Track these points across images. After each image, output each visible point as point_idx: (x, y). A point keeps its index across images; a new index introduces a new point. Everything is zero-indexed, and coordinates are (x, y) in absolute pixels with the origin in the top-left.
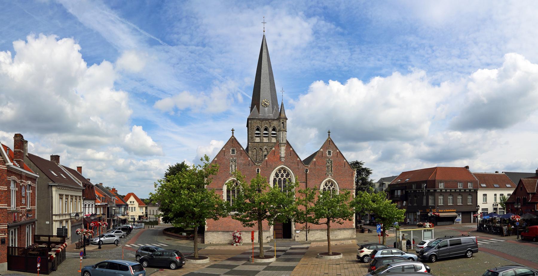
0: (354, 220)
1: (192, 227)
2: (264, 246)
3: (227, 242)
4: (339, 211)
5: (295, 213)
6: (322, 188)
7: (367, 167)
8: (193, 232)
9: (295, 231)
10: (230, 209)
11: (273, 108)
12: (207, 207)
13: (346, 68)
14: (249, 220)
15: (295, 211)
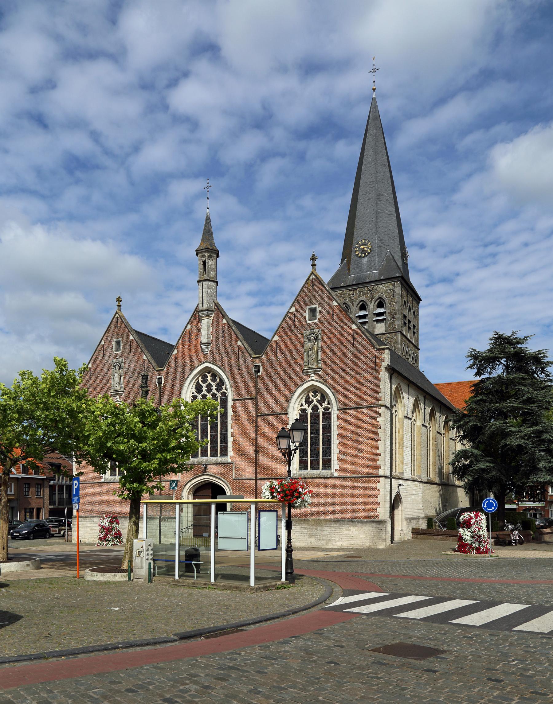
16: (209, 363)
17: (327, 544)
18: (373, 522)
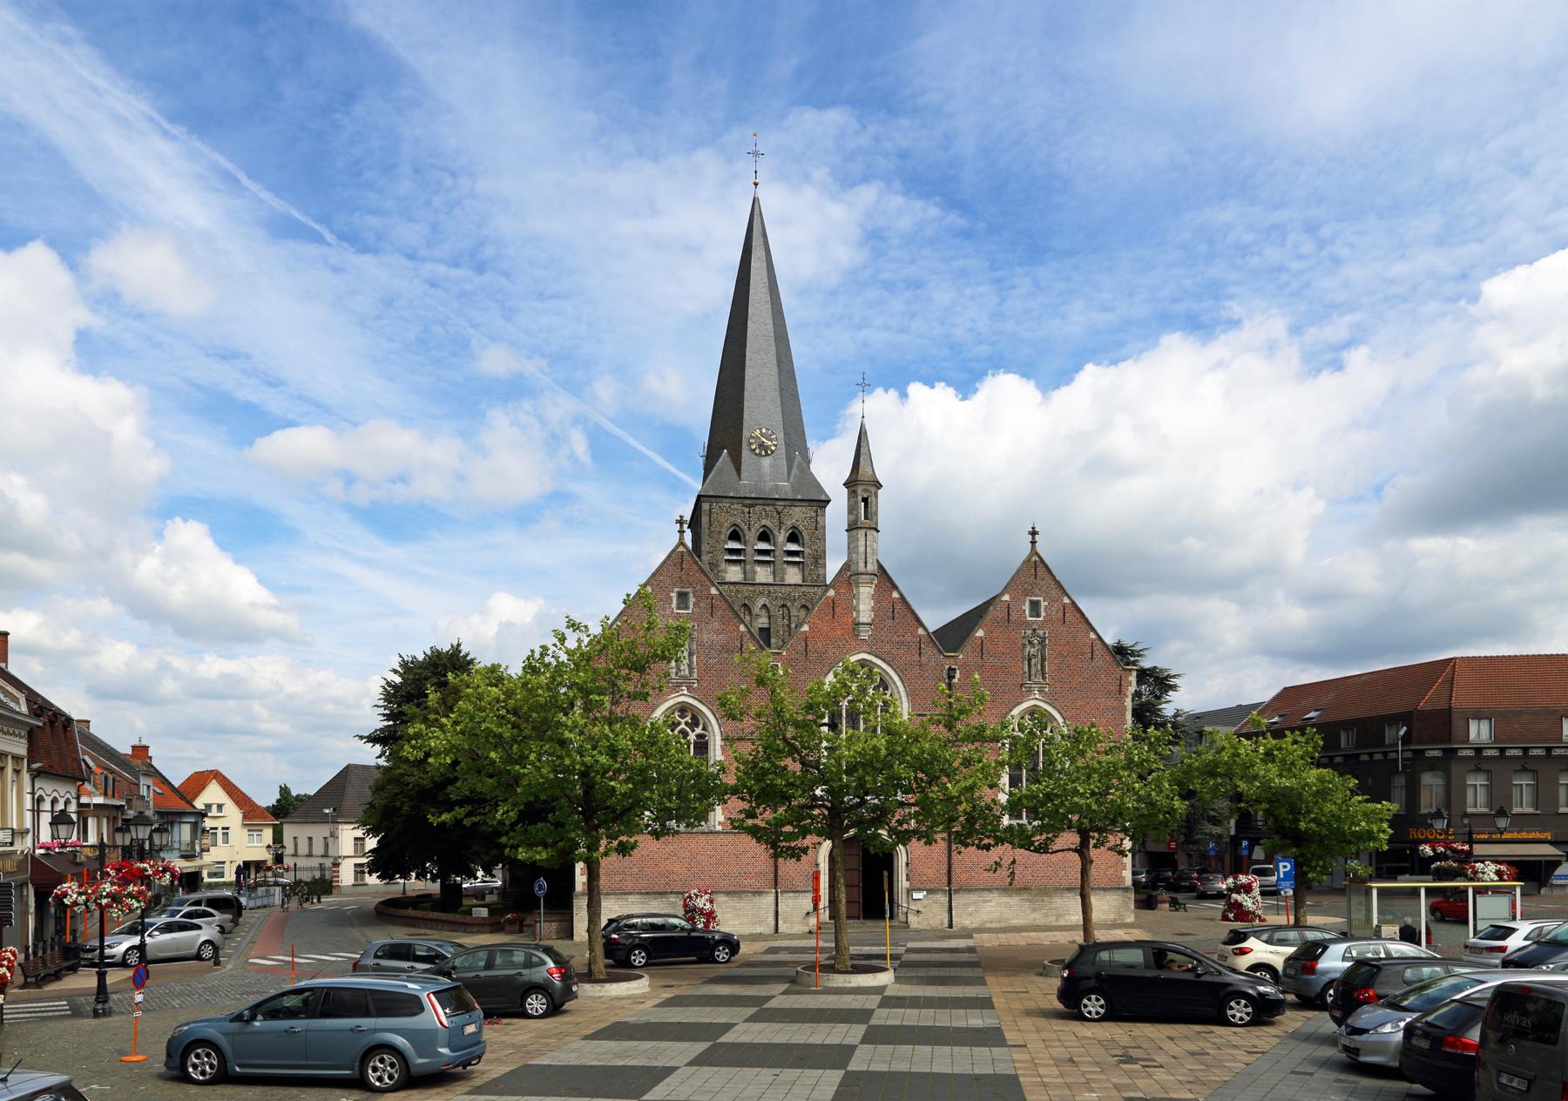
9: (909, 892)
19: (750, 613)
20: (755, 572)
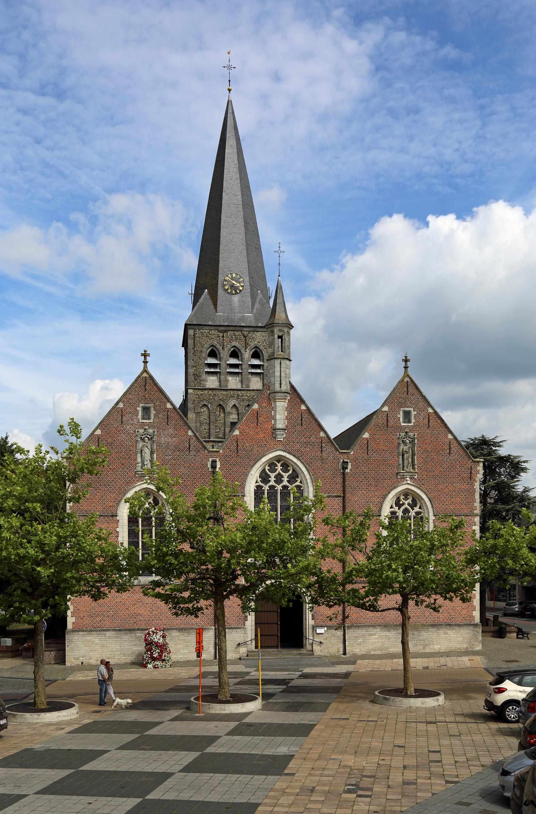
0: (476, 601)
1: (29, 623)
2: (230, 668)
3: (129, 659)
4: (434, 573)
5: (314, 579)
6: (386, 511)
7: (514, 453)
8: (31, 634)
9: (314, 628)
10: (138, 568)
11: (253, 297)
12: (75, 564)
13: (467, 168)
14: (190, 600)
15: (314, 574)
16: (284, 451)
17: (424, 649)
18: (470, 625)
19: (224, 411)
20: (227, 381)
